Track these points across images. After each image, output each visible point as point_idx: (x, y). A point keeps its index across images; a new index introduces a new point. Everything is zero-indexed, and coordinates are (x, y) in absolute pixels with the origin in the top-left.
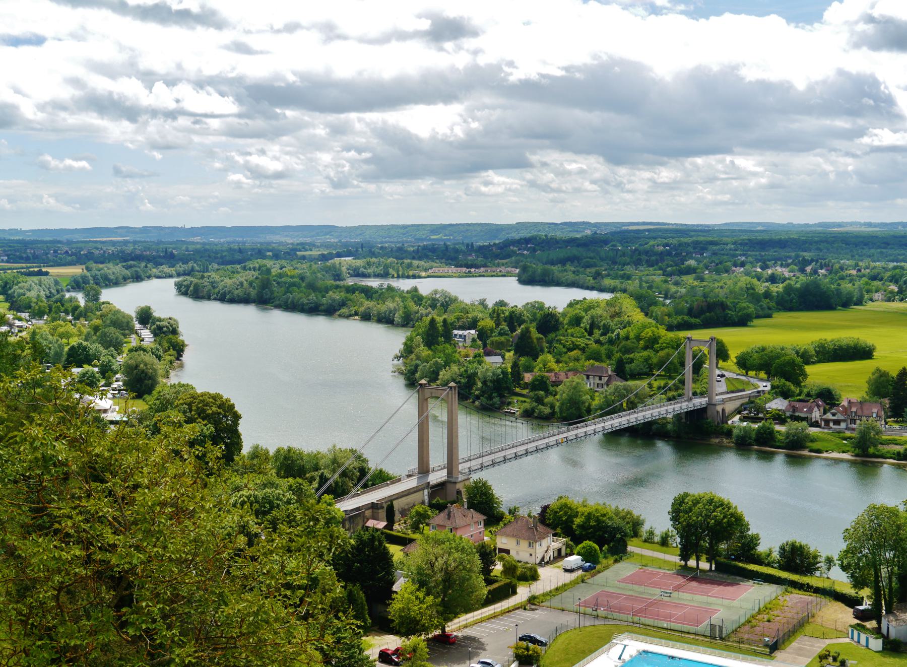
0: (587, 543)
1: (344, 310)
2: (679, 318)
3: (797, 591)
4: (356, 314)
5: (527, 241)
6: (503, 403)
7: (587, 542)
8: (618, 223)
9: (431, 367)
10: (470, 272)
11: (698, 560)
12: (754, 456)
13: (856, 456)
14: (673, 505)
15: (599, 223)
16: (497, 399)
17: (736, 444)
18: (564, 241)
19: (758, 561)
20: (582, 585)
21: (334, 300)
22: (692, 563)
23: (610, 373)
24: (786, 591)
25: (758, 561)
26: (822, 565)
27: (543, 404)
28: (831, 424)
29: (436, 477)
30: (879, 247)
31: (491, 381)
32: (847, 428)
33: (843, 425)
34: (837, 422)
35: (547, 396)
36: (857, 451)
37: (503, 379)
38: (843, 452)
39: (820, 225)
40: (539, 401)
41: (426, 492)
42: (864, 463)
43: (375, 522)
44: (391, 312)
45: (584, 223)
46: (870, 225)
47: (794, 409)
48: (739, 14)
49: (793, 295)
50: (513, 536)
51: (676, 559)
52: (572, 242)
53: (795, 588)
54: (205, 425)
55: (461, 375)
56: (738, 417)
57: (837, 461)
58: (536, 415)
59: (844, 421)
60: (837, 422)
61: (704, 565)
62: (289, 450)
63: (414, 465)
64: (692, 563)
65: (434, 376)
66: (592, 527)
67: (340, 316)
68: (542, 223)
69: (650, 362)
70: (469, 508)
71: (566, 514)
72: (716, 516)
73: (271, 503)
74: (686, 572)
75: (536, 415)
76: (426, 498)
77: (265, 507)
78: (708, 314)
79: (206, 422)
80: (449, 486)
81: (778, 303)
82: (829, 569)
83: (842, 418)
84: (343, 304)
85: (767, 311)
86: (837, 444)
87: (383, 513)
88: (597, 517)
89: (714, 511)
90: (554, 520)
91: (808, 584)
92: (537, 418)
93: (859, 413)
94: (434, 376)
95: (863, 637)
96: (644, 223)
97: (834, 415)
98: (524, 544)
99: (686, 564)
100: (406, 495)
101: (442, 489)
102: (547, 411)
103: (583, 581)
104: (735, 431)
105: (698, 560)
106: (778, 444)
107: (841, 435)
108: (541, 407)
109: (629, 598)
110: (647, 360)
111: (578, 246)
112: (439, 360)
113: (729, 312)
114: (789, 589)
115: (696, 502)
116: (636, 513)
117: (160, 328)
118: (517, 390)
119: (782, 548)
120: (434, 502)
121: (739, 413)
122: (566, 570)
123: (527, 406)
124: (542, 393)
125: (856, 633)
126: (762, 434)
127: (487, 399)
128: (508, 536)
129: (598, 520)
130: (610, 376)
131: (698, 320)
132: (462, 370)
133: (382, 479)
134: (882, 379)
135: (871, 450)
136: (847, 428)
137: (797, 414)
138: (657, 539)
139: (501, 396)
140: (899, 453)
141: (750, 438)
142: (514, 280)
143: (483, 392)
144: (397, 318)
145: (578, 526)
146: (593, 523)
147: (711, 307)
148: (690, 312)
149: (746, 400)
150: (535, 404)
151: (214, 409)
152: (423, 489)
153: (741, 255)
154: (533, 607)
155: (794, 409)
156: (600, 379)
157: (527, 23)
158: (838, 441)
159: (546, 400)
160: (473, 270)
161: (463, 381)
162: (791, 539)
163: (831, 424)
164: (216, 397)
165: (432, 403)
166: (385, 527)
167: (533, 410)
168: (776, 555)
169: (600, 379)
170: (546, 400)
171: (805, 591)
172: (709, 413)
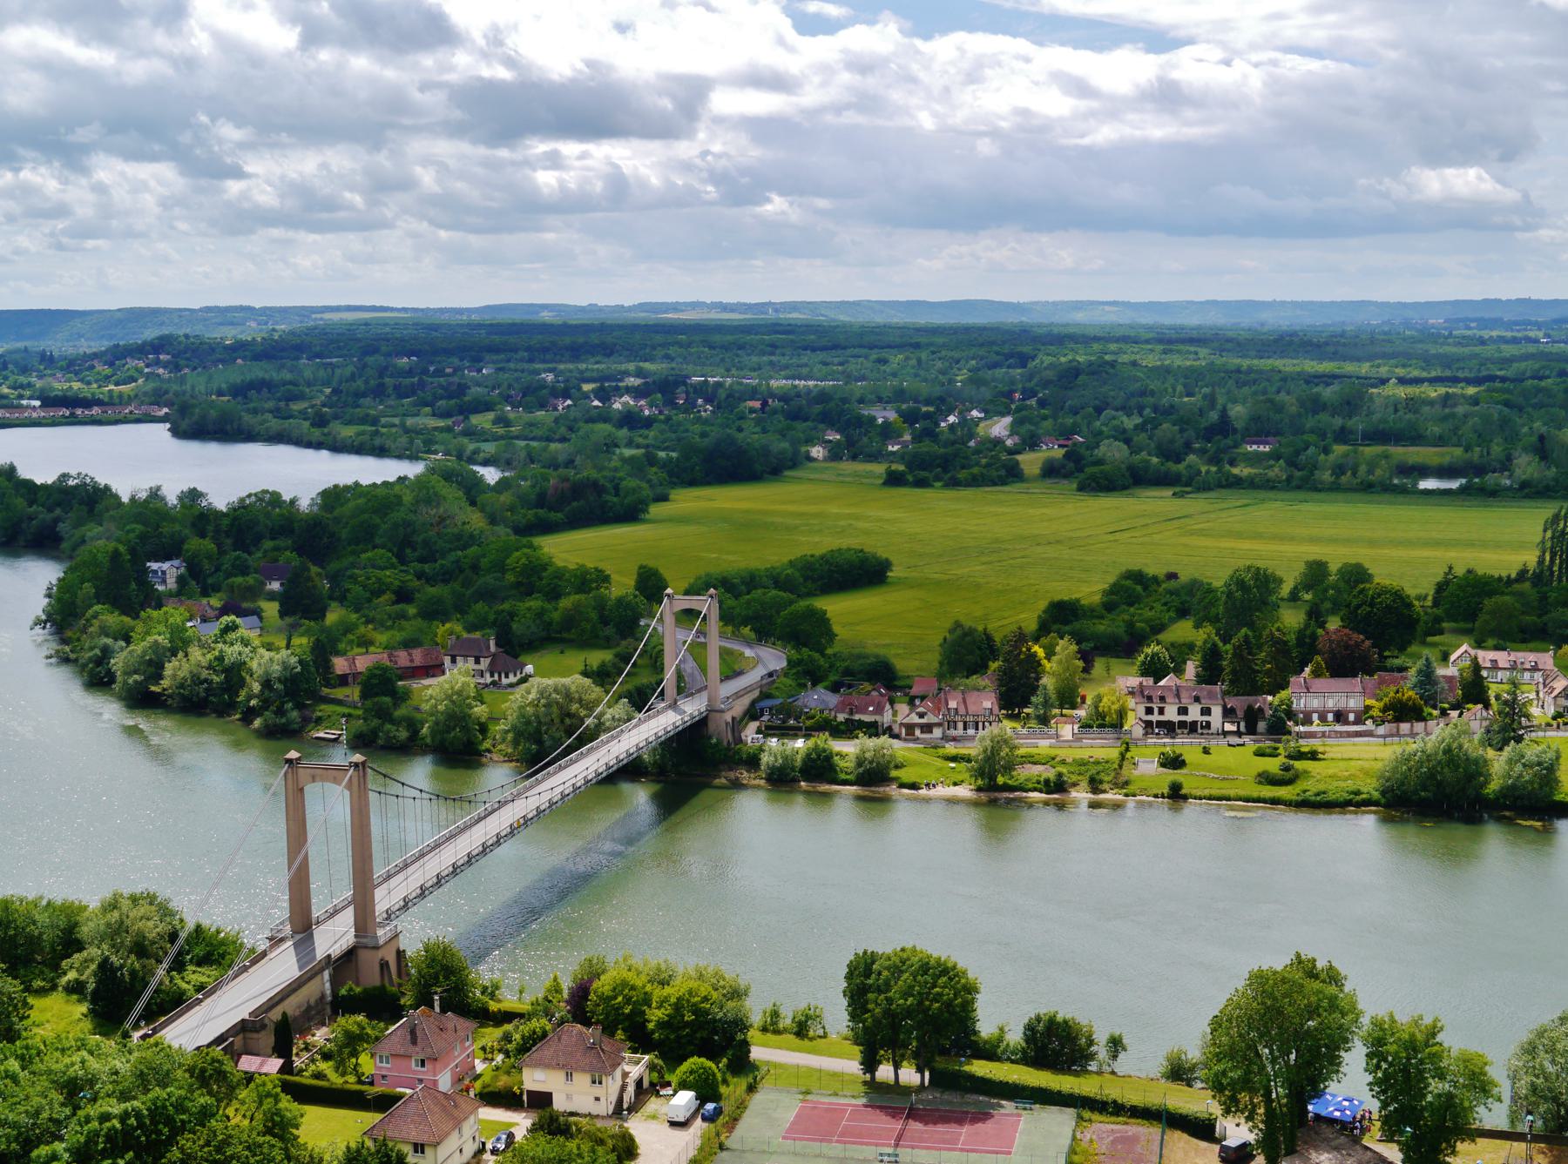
0: (694, 1062)
3: (1096, 1117)
5: (158, 346)
6: (306, 720)
7: (695, 1059)
8: (303, 308)
9: (144, 653)
10: (72, 414)
11: (897, 1067)
12: (800, 799)
13: (979, 790)
15: (270, 309)
16: (295, 714)
17: (769, 779)
19: (989, 1052)
20: (724, 1154)
22: (885, 1072)
23: (493, 648)
25: (989, 1052)
27: (392, 721)
28: (918, 732)
29: (334, 937)
30: (763, 353)
31: (279, 680)
32: (945, 738)
33: (937, 732)
34: (927, 728)
36: (980, 782)
37: (301, 674)
38: (955, 784)
39: (642, 307)
40: (384, 715)
41: (326, 974)
42: (993, 802)
45: (242, 309)
46: (724, 307)
48: (814, 35)
49: (695, 459)
50: (558, 1066)
53: (1092, 1109)
56: (754, 725)
57: (952, 801)
58: (380, 742)
59: (939, 725)
60: (927, 728)
61: (910, 1075)
63: (281, 912)
64: (885, 1072)
65: (152, 670)
66: (688, 1024)
69: (546, 618)
70: (444, 1010)
71: (628, 1000)
72: (941, 995)
73: (169, 1121)
75: (380, 742)
76: (328, 985)
77: (160, 1133)
78: (575, 504)
80: (364, 955)
82: (1115, 1057)
83: (936, 720)
85: (659, 490)
86: (940, 769)
87: (267, 1039)
88: (694, 1005)
89: (934, 986)
90: (607, 1015)
91: (1115, 1102)
92: (383, 748)
93: (962, 711)
94: (152, 670)
96: (349, 308)
97: (921, 715)
98: (582, 1080)
99: (873, 1078)
100: (295, 990)
101: (349, 961)
103: (722, 1147)
105: (897, 1067)
106: (843, 776)
107: (941, 751)
108: (388, 726)
112: (160, 639)
113: (608, 498)
114: (1087, 1114)
118: (325, 691)
120: (343, 992)
121: (754, 718)
124: (387, 699)
126: (813, 761)
127: (276, 713)
128: (547, 1066)
129: (696, 1011)
130: (494, 655)
131: (560, 515)
132: (209, 656)
133: (214, 954)
134: (968, 639)
135: (1000, 780)
136: (945, 738)
137: (857, 717)
138: (786, 1021)
139: (300, 706)
140: (1047, 782)
141: (793, 769)
142: (162, 430)
143: (266, 704)
145: (661, 1025)
146: (689, 1017)
148: (541, 501)
149: (756, 693)
150: (375, 722)
152: (322, 970)
153: (546, 371)
156: (477, 662)
158: (940, 763)
160: (79, 412)
161: (216, 679)
162: (1044, 1010)
163: (918, 732)
165: (313, 791)
167: (374, 733)
168: (1015, 1037)
169: (477, 662)
170: (398, 713)
171: (1112, 1114)
172: (712, 727)
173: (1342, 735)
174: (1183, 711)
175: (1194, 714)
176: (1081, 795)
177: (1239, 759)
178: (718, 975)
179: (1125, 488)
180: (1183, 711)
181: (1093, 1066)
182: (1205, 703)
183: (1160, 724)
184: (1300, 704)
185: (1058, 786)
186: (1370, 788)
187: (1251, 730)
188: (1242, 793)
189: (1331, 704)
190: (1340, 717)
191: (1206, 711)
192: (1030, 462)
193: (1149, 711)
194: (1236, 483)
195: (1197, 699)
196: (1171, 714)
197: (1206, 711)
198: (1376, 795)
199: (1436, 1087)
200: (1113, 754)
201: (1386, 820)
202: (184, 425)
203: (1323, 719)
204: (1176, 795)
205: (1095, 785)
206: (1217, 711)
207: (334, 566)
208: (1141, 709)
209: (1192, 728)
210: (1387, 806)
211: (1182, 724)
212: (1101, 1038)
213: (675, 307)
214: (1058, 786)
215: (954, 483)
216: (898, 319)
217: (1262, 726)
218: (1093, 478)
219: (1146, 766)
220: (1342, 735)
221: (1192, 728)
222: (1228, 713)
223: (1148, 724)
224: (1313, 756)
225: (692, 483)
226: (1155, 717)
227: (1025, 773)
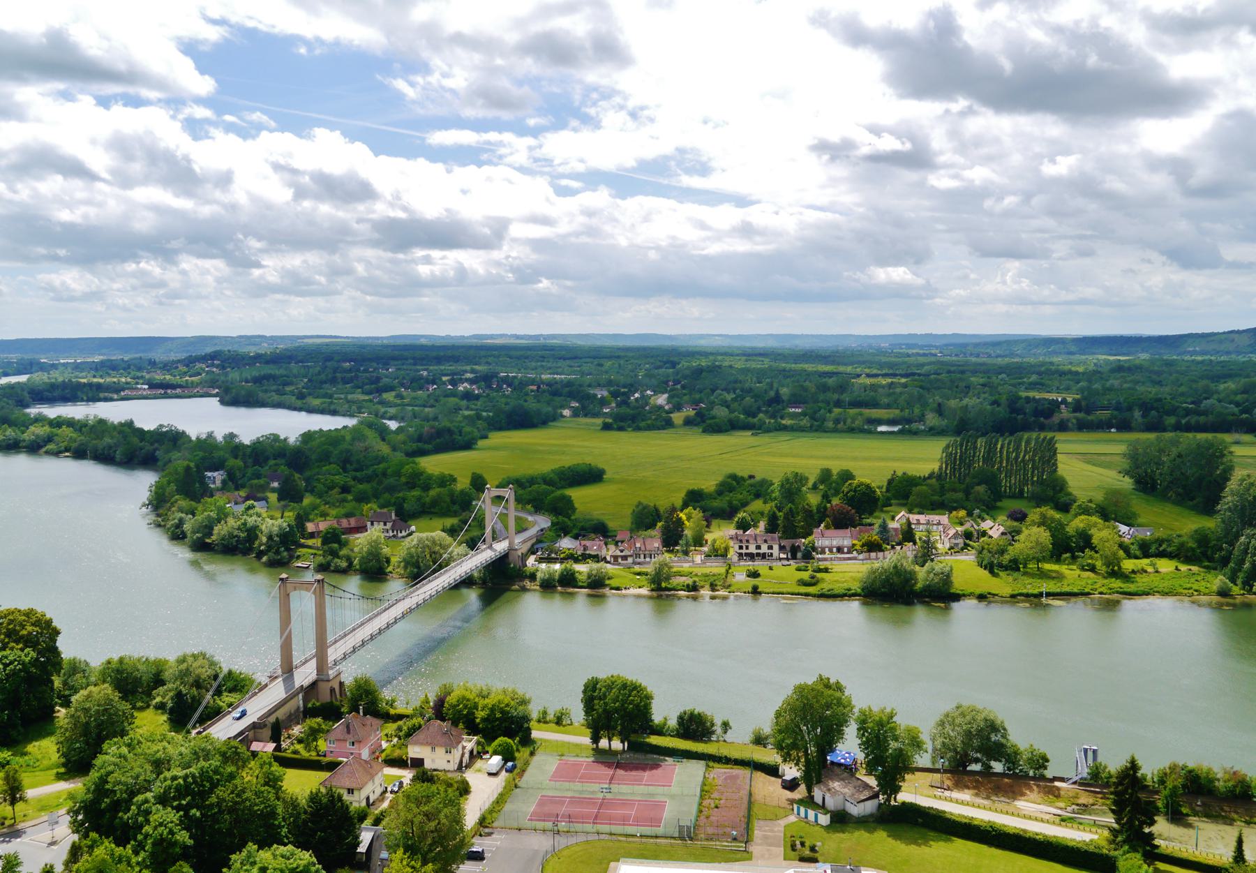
0: (501, 740)
1: (51, 446)
2: (414, 446)
4: (67, 450)
6: (291, 557)
11: (610, 740)
14: (584, 692)
16: (285, 554)
17: (541, 586)
18: (251, 357)
21: (37, 436)
22: (604, 743)
24: (708, 766)
25: (659, 731)
26: (718, 729)
27: (338, 557)
29: (305, 675)
33: (630, 560)
35: (340, 549)
40: (335, 554)
41: (300, 696)
42: (659, 597)
43: (261, 744)
44: (110, 447)
45: (260, 336)
46: (517, 337)
47: (585, 548)
50: (427, 744)
51: (586, 740)
52: (258, 358)
54: (22, 650)
55: (239, 529)
57: (639, 596)
60: (625, 558)
61: (617, 745)
62: (121, 661)
63: (276, 663)
66: (498, 719)
67: (47, 453)
68: (218, 337)
70: (365, 714)
71: (466, 707)
73: (210, 779)
74: (604, 757)
77: (204, 786)
79: (21, 646)
81: (489, 424)
84: (49, 439)
95: (811, 814)
98: (440, 751)
102: (344, 564)
103: (516, 786)
104: (539, 575)
105: (610, 740)
109: (574, 801)
110: (419, 499)
111: (267, 362)
114: (711, 764)
115: (609, 688)
116: (520, 692)
117: (424, 773)
119: (681, 718)
121: (533, 553)
122: (490, 774)
123: (320, 559)
124: (336, 545)
125: (795, 806)
129: (503, 712)
136: (634, 563)
138: (550, 717)
139: (288, 549)
143: (269, 548)
144: (118, 457)
147: (439, 433)
148: (420, 439)
151: (29, 628)
154: (487, 830)
155: (585, 548)
157: (464, 192)
158: (632, 576)
159: (342, 553)
164: (29, 613)
166: (275, 750)
167: (329, 564)
170: (342, 553)
172: (511, 558)
173: (840, 559)
174: (758, 547)
175: (764, 549)
176: (706, 592)
177: (787, 572)
178: (514, 692)
179: (727, 431)
180: (758, 547)
181: (714, 738)
182: (770, 543)
183: (746, 554)
184: (819, 543)
185: (694, 588)
186: (856, 587)
187: (794, 557)
188: (790, 590)
189: (835, 543)
190: (840, 550)
191: (770, 548)
192: (678, 418)
193: (741, 548)
194: (785, 428)
195: (766, 541)
196: (752, 549)
197: (770, 548)
198: (859, 591)
199: (893, 745)
200: (723, 570)
201: (865, 604)
202: (227, 398)
203: (831, 551)
204: (755, 591)
205: (713, 587)
206: (776, 547)
207: (308, 473)
208: (737, 547)
209: (763, 556)
210: (865, 596)
211: (758, 554)
212: (718, 722)
213: (492, 337)
214: (694, 588)
215: (638, 429)
216: (608, 343)
217: (799, 555)
218: (710, 425)
219: (740, 577)
220: (840, 559)
221: (763, 556)
222: (782, 548)
223: (741, 555)
224: (826, 570)
225: (500, 429)
226: (744, 551)
227: (676, 581)
